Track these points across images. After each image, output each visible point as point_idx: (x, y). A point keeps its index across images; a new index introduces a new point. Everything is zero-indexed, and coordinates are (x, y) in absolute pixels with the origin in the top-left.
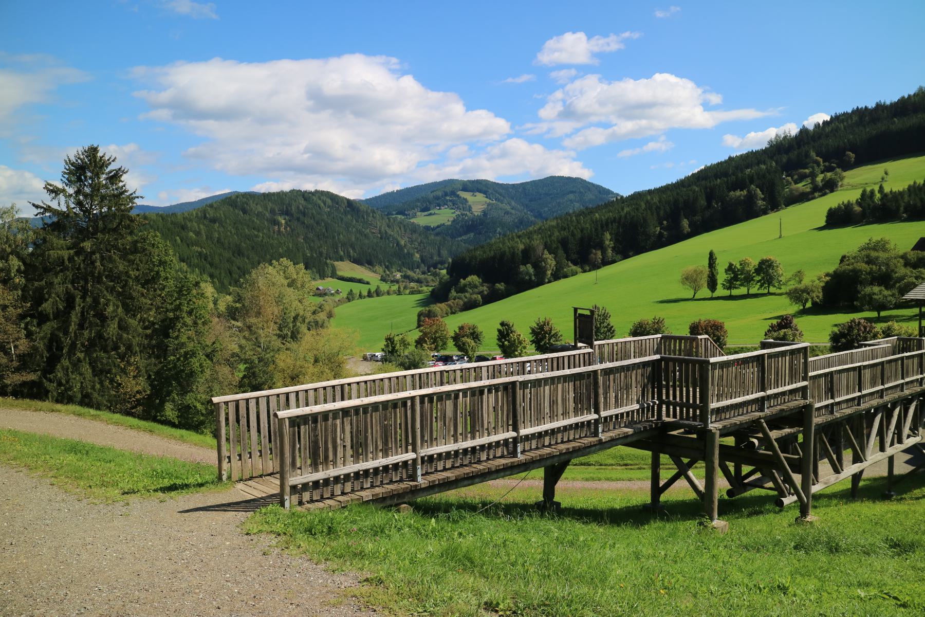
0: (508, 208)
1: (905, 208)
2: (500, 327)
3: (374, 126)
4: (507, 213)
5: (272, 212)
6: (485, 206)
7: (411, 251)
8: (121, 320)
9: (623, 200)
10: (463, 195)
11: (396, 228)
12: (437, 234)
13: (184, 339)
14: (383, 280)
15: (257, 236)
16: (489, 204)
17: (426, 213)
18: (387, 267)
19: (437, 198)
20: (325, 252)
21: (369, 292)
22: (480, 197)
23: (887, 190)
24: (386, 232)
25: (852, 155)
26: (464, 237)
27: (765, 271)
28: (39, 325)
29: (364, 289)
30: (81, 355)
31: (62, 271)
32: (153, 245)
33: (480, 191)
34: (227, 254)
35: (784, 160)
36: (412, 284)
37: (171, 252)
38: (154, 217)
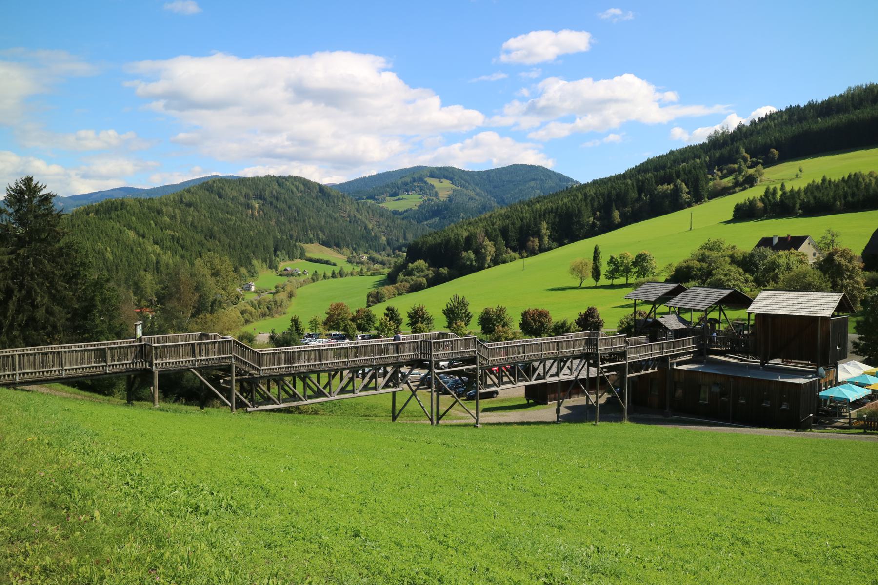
0: (472, 194)
1: (801, 205)
2: (386, 312)
3: (353, 117)
4: (471, 199)
5: (247, 196)
6: (451, 192)
7: (378, 234)
9: (582, 187)
10: (430, 181)
11: (365, 213)
12: (403, 219)
13: (97, 321)
14: (350, 261)
15: (230, 220)
17: (395, 198)
18: (354, 249)
19: (406, 184)
20: (295, 235)
21: (333, 273)
22: (446, 183)
23: (788, 188)
24: (355, 217)
25: (776, 152)
26: (429, 222)
27: (641, 262)
29: (328, 270)
30: (16, 333)
33: (446, 178)
34: (198, 237)
35: (717, 155)
36: (376, 266)
38: (132, 203)
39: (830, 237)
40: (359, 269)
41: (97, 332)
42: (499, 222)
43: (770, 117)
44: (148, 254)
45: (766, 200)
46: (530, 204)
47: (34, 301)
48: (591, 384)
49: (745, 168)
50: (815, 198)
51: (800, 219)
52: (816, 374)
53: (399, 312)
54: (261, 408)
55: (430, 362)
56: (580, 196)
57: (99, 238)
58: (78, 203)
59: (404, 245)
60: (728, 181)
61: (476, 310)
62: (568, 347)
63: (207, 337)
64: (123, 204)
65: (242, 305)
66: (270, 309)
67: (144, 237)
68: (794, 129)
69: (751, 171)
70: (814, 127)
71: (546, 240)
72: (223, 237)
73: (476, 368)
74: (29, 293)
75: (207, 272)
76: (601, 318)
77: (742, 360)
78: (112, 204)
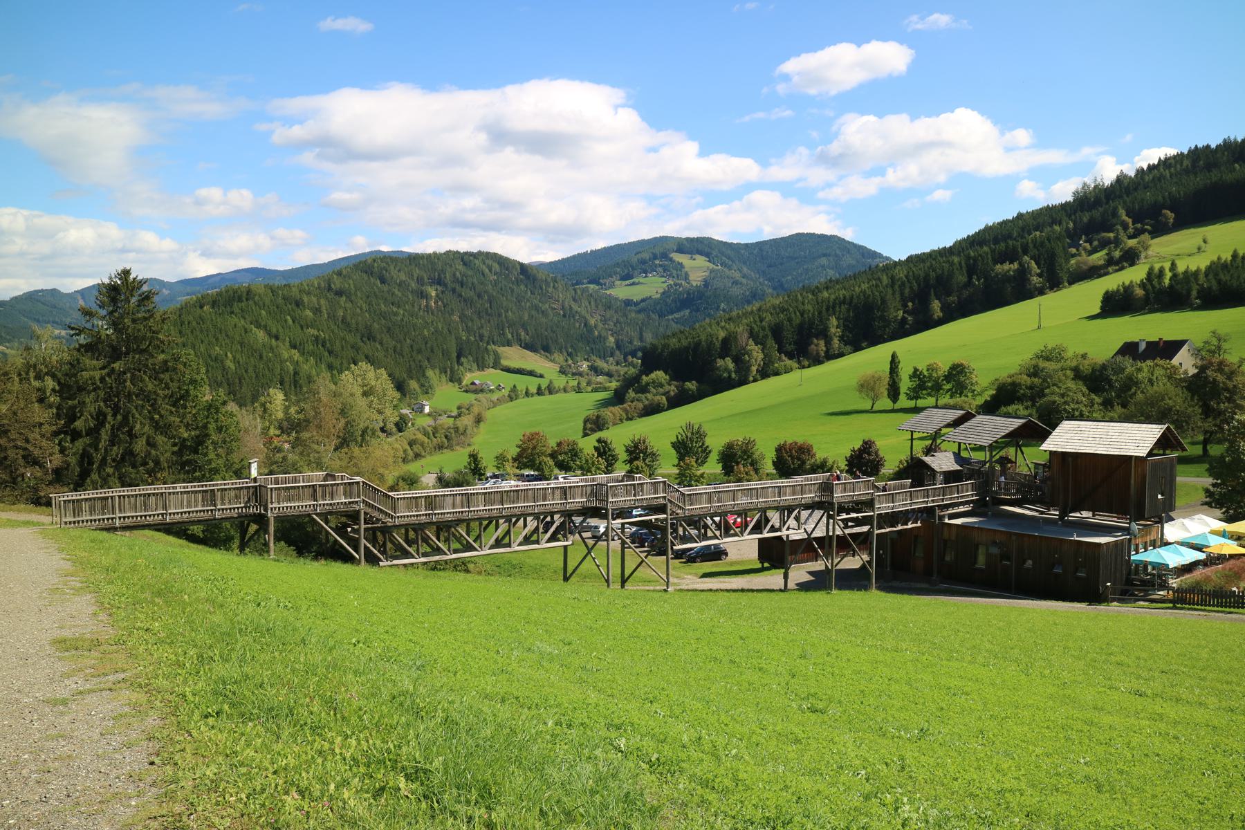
0: (737, 275)
3: (570, 169)
4: (736, 283)
5: (420, 281)
7: (604, 333)
8: (148, 438)
10: (678, 258)
11: (585, 303)
12: (639, 312)
13: (212, 455)
14: (562, 372)
15: (396, 314)
16: (712, 271)
17: (628, 282)
18: (570, 355)
19: (643, 262)
20: (486, 334)
21: (539, 388)
22: (701, 261)
23: (1181, 268)
24: (571, 308)
25: (1170, 215)
28: (72, 441)
29: (532, 383)
30: (109, 470)
31: (94, 390)
32: (185, 364)
33: (701, 253)
34: (351, 338)
35: (1085, 220)
36: (600, 379)
37: (203, 370)
38: (262, 291)
39: (1215, 342)
40: (575, 383)
41: (211, 470)
42: (769, 318)
43: (1165, 163)
44: (282, 362)
45: (1149, 287)
46: (815, 291)
47: (131, 429)
48: (844, 545)
49: (1125, 238)
50: (1219, 282)
51: (1197, 313)
52: (1127, 530)
53: (613, 446)
54: (396, 562)
55: (607, 510)
56: (885, 280)
57: (217, 339)
58: (189, 289)
59: (640, 349)
60: (1098, 258)
61: (716, 442)
62: (845, 491)
63: (333, 477)
64: (249, 292)
65: (410, 433)
66: (448, 439)
67: (277, 338)
68: (1200, 181)
69: (1132, 243)
70: (1229, 177)
71: (836, 342)
72: (387, 339)
73: (666, 519)
74: (125, 418)
75: (358, 391)
76: (881, 454)
77: (1042, 513)
78: (235, 292)
